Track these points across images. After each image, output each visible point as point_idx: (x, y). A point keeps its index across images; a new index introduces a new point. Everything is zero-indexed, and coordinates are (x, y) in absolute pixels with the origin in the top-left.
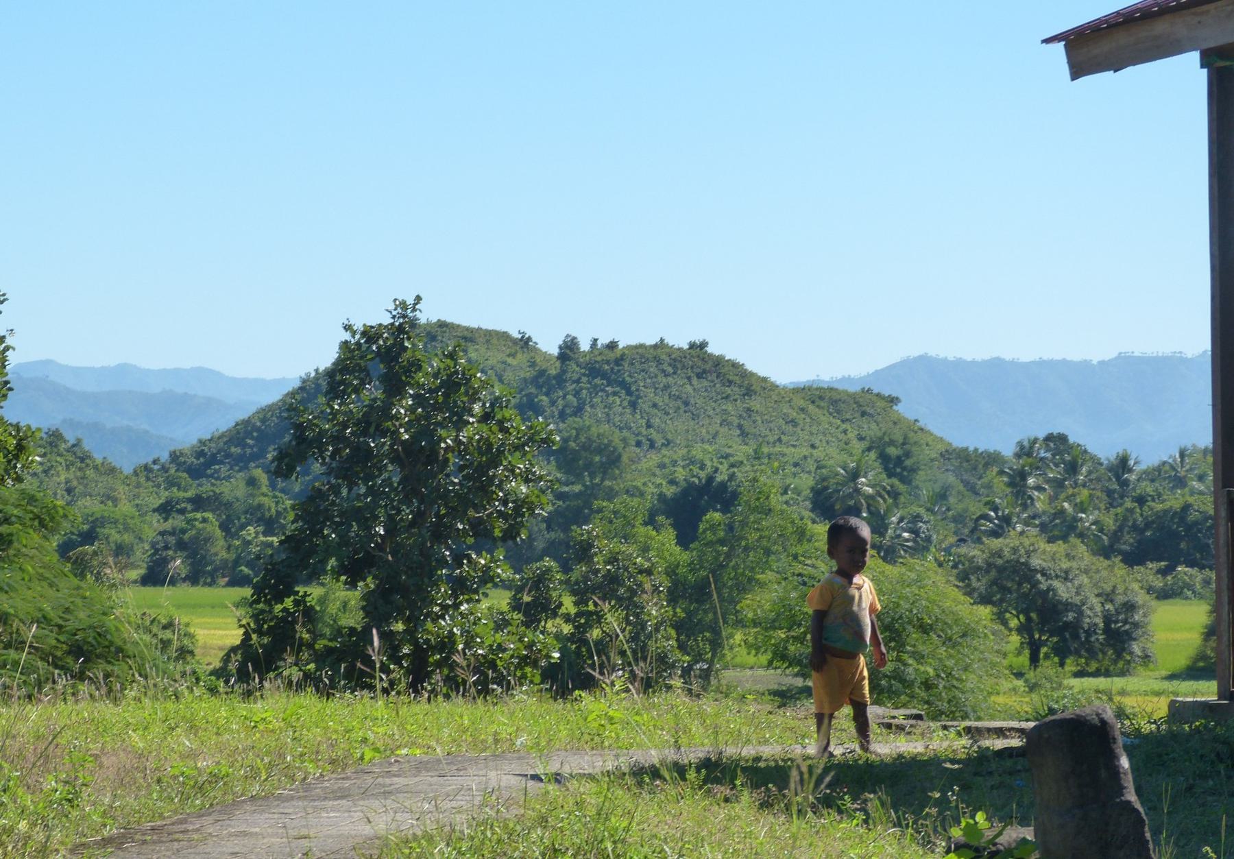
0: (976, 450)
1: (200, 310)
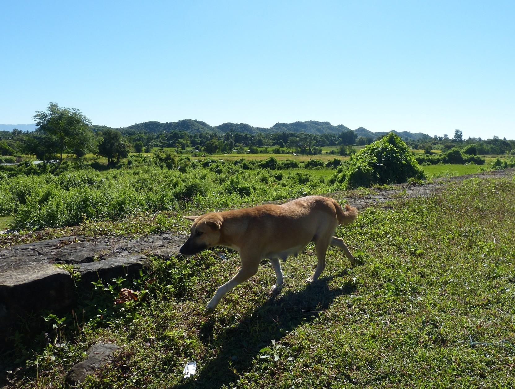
0: (480, 139)
1: (20, 114)
